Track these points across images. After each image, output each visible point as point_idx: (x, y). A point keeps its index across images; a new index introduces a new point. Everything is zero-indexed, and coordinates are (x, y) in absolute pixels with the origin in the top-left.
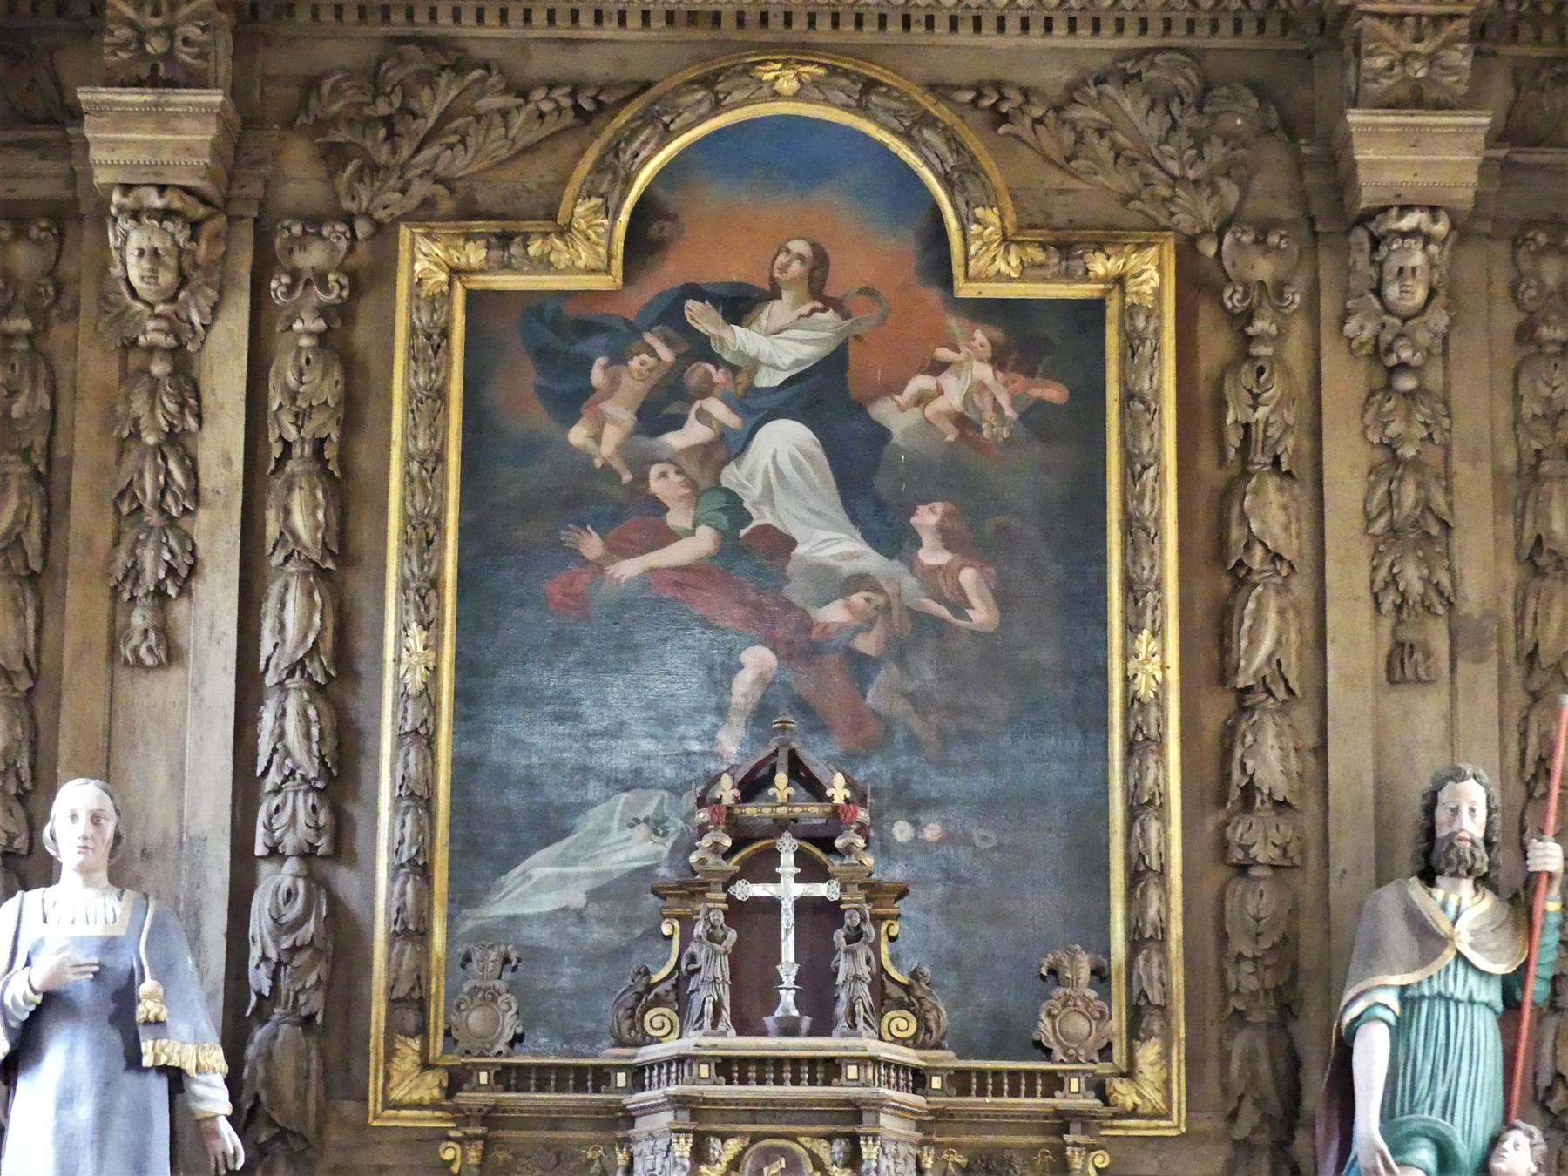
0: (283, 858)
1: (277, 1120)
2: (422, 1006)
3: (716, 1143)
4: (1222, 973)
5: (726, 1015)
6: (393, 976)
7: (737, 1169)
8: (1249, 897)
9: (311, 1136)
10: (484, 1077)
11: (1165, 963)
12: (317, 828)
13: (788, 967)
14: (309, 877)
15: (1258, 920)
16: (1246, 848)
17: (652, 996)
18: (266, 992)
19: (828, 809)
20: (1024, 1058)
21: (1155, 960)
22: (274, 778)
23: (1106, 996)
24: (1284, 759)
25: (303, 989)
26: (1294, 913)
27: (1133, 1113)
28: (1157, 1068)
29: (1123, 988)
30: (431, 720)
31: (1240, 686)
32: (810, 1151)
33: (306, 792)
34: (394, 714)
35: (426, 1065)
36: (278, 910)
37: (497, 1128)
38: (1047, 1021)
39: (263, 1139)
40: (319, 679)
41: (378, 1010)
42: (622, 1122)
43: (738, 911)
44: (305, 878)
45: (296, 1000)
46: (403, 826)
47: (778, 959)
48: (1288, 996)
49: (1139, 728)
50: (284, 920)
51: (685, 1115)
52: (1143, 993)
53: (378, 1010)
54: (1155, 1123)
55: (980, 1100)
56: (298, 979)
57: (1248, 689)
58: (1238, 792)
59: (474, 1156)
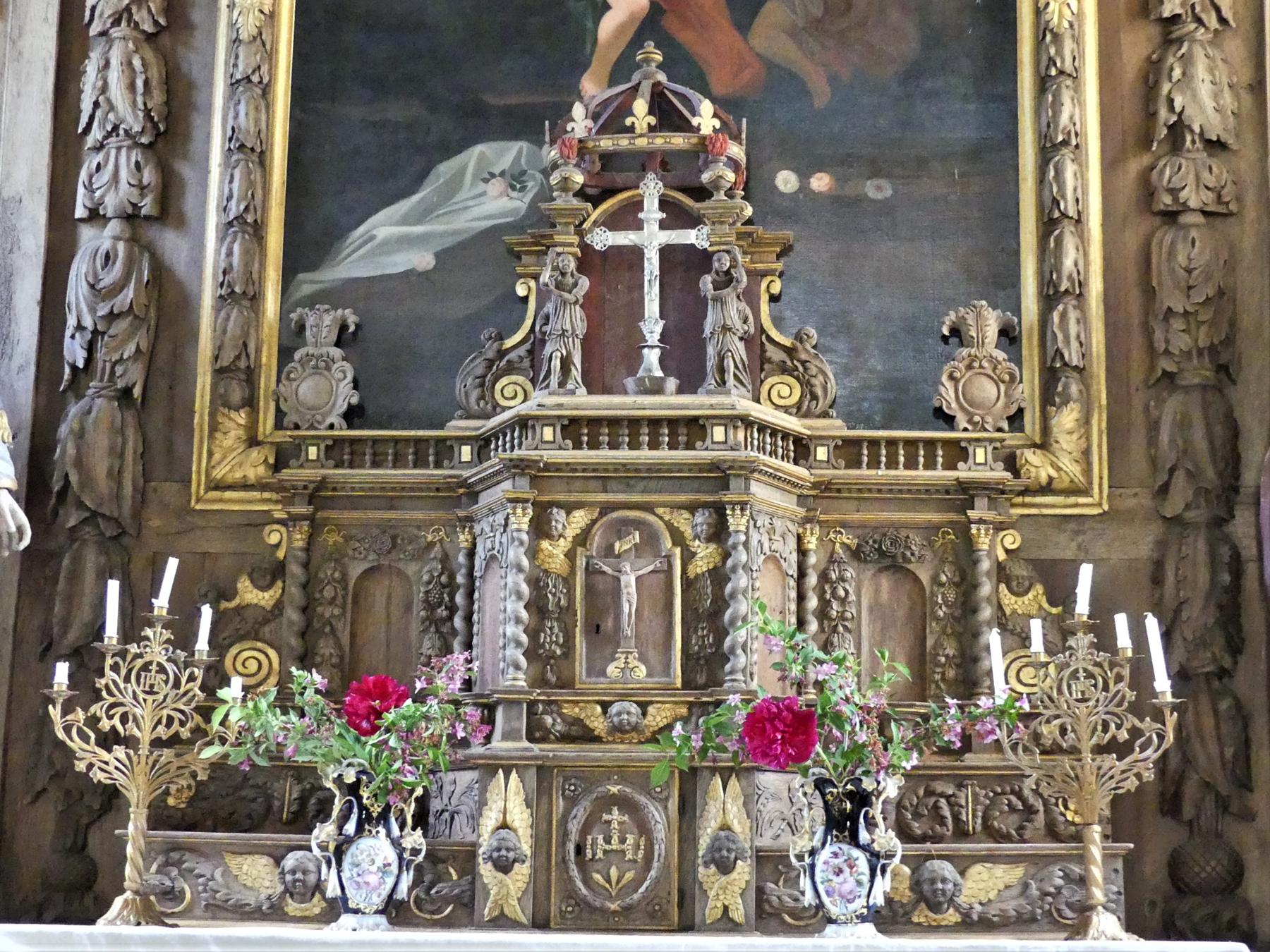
0: (105, 220)
1: (88, 503)
2: (250, 377)
3: (559, 515)
4: (1148, 332)
5: (576, 373)
6: (218, 343)
7: (584, 544)
8: (1180, 246)
9: (126, 519)
10: (313, 452)
11: (1083, 320)
12: (142, 188)
13: (652, 328)
14: (133, 240)
15: (1189, 271)
16: (1174, 192)
17: (504, 363)
18: (81, 364)
19: (694, 140)
20: (923, 428)
21: (1073, 315)
22: (96, 134)
23: (1017, 359)
24: (1216, 96)
25: (121, 360)
26: (1230, 266)
27: (1047, 489)
28: (1075, 437)
29: (1036, 351)
30: (265, 68)
31: (1166, 14)
32: (669, 525)
33: (130, 148)
34: (226, 63)
35: (253, 441)
36: (95, 275)
37: (323, 508)
38: (949, 385)
39: (72, 522)
40: (148, 27)
41: (204, 381)
42: (464, 499)
43: (588, 260)
44: (127, 241)
45: (113, 372)
46: (231, 182)
47: (641, 316)
48: (1224, 359)
49: (1052, 61)
50: (102, 284)
51: (524, 482)
52: (1059, 353)
53: (204, 381)
54: (1072, 500)
55: (872, 472)
56: (116, 349)
57: (1175, 19)
58: (1165, 131)
59: (299, 540)
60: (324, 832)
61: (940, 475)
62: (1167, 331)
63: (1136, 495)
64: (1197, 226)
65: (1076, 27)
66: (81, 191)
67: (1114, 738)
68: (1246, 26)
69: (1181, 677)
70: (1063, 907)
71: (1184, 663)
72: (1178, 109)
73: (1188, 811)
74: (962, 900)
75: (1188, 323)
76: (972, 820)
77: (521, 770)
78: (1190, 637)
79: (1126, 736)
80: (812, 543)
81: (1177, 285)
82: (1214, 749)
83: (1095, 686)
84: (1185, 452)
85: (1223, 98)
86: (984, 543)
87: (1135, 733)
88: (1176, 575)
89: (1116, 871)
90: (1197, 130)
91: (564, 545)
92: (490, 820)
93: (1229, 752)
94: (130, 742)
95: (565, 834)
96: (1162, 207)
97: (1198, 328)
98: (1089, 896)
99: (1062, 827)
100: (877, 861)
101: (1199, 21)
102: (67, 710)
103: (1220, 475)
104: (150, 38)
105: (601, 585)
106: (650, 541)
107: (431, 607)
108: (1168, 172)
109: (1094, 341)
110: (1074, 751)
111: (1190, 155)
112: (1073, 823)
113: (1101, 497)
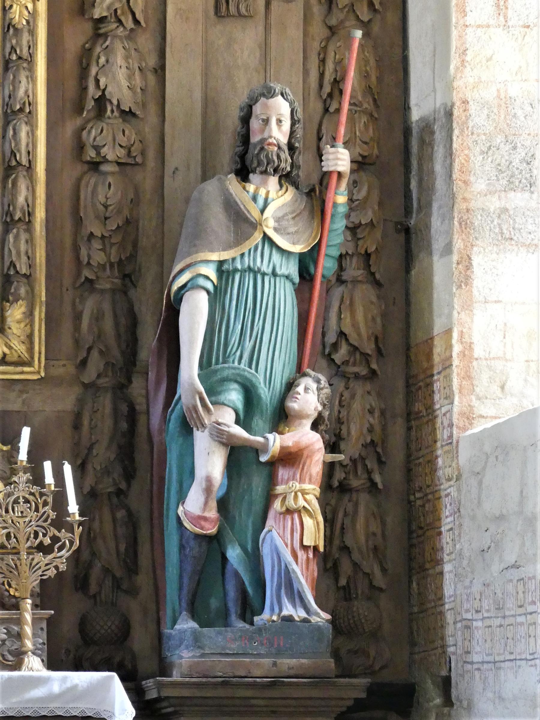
4: (76, 249)
8: (100, 189)
11: (30, 241)
15: (106, 207)
21: (23, 237)
24: (130, 77)
26: (135, 202)
31: (96, 16)
48: (128, 269)
49: (13, 48)
54: (19, 369)
57: (102, 20)
58: (93, 103)
62: (90, 249)
63: (64, 365)
64: (113, 173)
65: (31, 24)
67: (41, 543)
68: (153, 24)
70: (6, 653)
71: (93, 485)
72: (102, 87)
73: (93, 588)
75: (104, 244)
78: (98, 468)
79: (49, 541)
81: (97, 217)
82: (112, 545)
83: (30, 508)
84: (99, 336)
85: (135, 79)
87: (55, 539)
88: (90, 424)
89: (42, 629)
90: (115, 102)
93: (122, 547)
96: (89, 159)
97: (111, 248)
98: (23, 645)
99: (7, 599)
101: (120, 21)
103: (123, 353)
108: (93, 132)
109: (38, 255)
111: (110, 121)
112: (14, 597)
113: (40, 367)
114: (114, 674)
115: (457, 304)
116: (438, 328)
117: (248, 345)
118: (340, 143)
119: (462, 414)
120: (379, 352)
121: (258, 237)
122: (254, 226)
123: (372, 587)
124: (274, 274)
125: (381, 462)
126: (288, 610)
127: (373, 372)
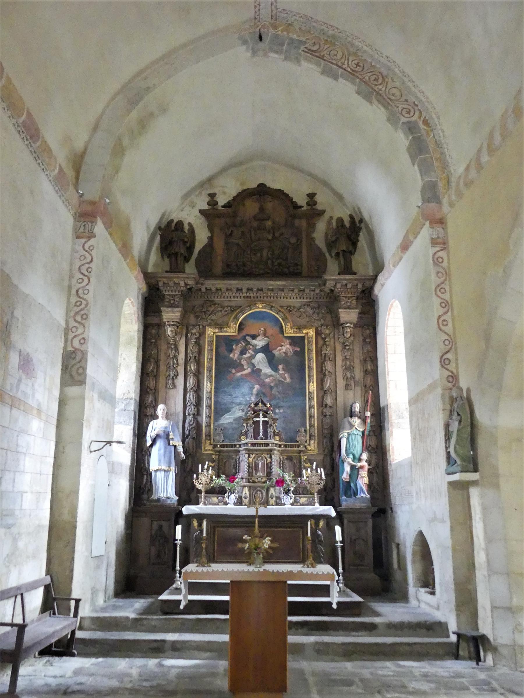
2: (210, 436)
3: (251, 455)
5: (253, 437)
14: (194, 418)
21: (313, 429)
22: (189, 404)
23: (306, 434)
24: (331, 400)
27: (310, 451)
35: (210, 444)
60: (226, 495)
61: (297, 449)
66: (187, 411)
69: (325, 475)
74: (300, 502)
76: (301, 492)
77: (248, 487)
80: (281, 458)
86: (302, 458)
87: (320, 482)
91: (252, 459)
92: (244, 493)
94: (202, 484)
95: (253, 494)
100: (291, 497)
102: (195, 480)
104: (195, 391)
105: (256, 464)
106: (262, 458)
107: (234, 465)
110: (313, 485)
114: (332, 507)
115: (390, 439)
116: (387, 443)
117: (353, 447)
118: (368, 411)
119: (392, 459)
120: (377, 448)
121: (354, 428)
122: (354, 426)
123: (378, 491)
124: (357, 434)
125: (378, 468)
126: (362, 495)
127: (376, 452)
